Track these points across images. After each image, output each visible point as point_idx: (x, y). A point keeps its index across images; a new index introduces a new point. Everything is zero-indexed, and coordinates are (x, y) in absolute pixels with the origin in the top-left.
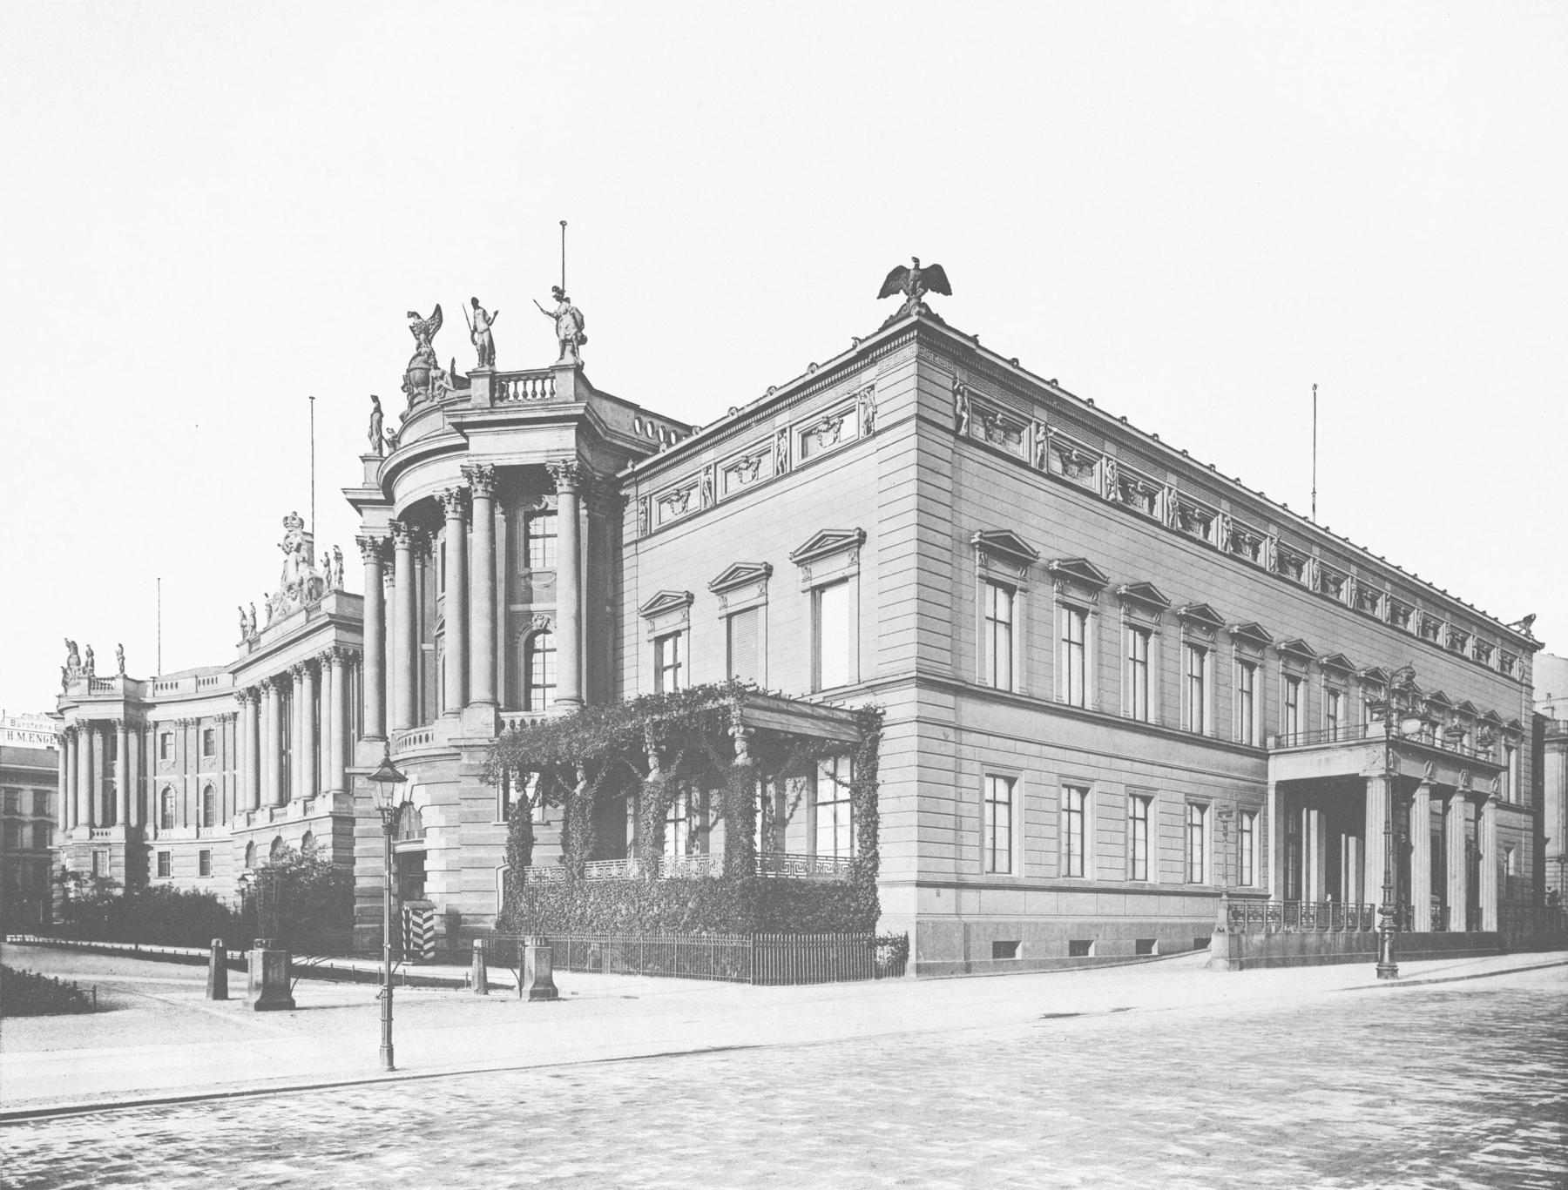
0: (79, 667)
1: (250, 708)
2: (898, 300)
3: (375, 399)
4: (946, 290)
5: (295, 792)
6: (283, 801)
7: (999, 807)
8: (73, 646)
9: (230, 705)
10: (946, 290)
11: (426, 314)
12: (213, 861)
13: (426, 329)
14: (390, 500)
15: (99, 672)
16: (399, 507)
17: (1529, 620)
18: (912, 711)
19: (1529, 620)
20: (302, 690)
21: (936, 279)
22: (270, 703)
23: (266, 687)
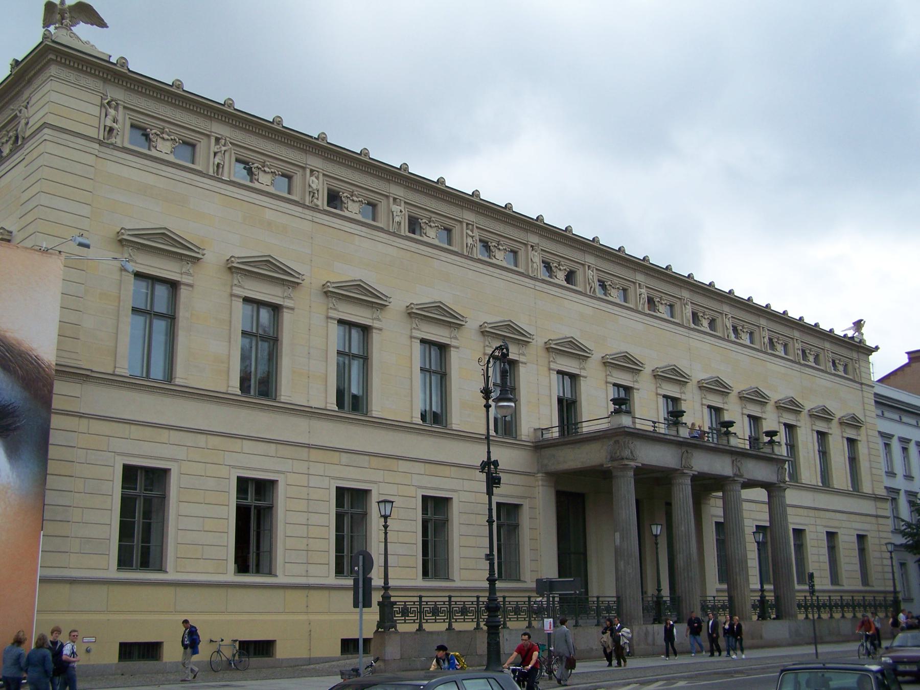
4: (100, 23)
17: (858, 325)
19: (858, 325)
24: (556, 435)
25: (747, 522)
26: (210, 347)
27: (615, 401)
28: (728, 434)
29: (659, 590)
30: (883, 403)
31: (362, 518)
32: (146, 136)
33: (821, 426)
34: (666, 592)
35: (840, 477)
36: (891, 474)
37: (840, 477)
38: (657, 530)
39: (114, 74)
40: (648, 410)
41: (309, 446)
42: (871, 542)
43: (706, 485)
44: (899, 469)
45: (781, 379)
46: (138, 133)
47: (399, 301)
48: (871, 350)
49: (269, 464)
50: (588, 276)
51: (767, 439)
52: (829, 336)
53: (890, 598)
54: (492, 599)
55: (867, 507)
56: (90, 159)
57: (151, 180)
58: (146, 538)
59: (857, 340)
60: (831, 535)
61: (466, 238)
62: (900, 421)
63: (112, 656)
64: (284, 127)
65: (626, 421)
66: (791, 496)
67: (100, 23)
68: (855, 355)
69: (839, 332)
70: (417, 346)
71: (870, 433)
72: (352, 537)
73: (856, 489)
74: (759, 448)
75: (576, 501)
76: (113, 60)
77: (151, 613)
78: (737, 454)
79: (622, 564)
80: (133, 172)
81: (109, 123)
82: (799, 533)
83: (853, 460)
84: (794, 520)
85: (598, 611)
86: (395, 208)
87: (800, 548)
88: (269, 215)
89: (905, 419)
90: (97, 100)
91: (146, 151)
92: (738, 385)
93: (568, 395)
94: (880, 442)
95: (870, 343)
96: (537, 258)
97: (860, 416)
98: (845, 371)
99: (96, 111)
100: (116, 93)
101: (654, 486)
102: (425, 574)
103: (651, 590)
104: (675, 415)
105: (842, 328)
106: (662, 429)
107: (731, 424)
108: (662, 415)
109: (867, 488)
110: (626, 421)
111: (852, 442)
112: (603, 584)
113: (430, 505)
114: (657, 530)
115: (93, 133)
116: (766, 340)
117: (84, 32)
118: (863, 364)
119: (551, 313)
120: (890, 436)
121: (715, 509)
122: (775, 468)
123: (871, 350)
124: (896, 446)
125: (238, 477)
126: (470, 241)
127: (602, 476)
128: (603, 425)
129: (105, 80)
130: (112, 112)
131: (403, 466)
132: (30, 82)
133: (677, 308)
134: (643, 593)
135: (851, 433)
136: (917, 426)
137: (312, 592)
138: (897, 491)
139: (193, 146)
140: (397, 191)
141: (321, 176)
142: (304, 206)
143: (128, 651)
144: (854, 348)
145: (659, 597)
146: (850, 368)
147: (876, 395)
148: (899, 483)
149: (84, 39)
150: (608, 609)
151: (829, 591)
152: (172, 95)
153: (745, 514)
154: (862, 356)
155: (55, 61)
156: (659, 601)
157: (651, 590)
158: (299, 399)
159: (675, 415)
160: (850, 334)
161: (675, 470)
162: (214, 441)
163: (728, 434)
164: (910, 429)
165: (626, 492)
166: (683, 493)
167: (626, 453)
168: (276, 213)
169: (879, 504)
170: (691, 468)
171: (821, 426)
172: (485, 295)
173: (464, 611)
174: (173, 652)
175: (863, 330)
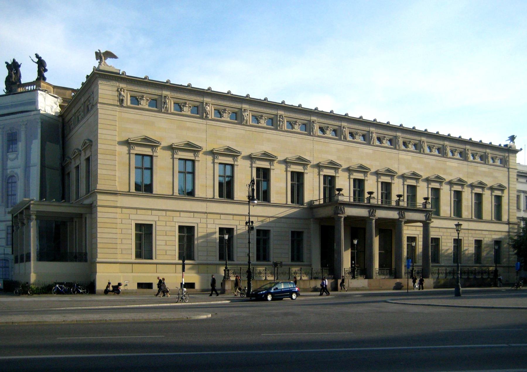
4: (114, 57)
19: (512, 138)
21: (109, 55)
26: (206, 182)
46: (217, 111)
48: (515, 152)
49: (191, 220)
50: (248, 116)
51: (337, 192)
57: (137, 117)
59: (509, 146)
63: (135, 287)
64: (232, 95)
66: (435, 223)
67: (114, 57)
72: (140, 249)
77: (149, 274)
80: (132, 115)
88: (188, 124)
95: (518, 148)
105: (500, 140)
109: (505, 218)
113: (261, 233)
117: (109, 61)
125: (179, 226)
141: (211, 105)
143: (141, 285)
149: (109, 65)
151: (452, 266)
155: (99, 77)
158: (203, 195)
160: (508, 142)
174: (155, 287)
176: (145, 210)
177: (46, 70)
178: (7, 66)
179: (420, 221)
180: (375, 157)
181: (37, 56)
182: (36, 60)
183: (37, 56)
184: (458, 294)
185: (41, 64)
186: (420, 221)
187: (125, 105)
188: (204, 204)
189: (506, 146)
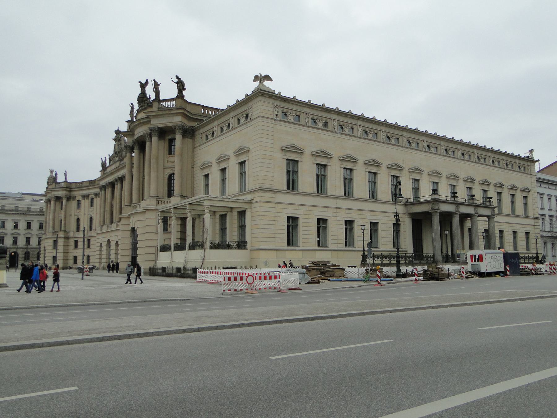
0: (53, 180)
1: (103, 192)
2: (258, 83)
3: (132, 104)
4: (271, 80)
5: (114, 220)
6: (112, 222)
7: (59, 236)
8: (52, 172)
9: (97, 190)
10: (271, 80)
11: (143, 82)
12: (91, 243)
13: (143, 86)
14: (133, 135)
15: (58, 181)
16: (136, 137)
17: (531, 151)
18: (63, 236)
19: (531, 151)
20: (118, 186)
21: (267, 78)
22: (109, 190)
23: (150, 136)
24: (412, 201)
25: (479, 231)
27: (433, 190)
28: (473, 199)
29: (447, 252)
30: (540, 181)
31: (352, 229)
32: (286, 115)
33: (513, 192)
34: (450, 252)
35: (519, 210)
36: (543, 209)
37: (519, 210)
38: (447, 232)
39: (278, 98)
40: (444, 193)
41: (337, 208)
42: (531, 237)
43: (464, 217)
44: (546, 206)
45: (496, 175)
47: (361, 159)
48: (535, 162)
52: (518, 157)
53: (535, 255)
54: (398, 254)
55: (531, 222)
56: (272, 125)
58: (39, 215)
60: (515, 233)
61: (382, 136)
62: (548, 188)
65: (436, 196)
68: (529, 164)
69: (522, 155)
70: (367, 174)
71: (533, 193)
73: (526, 216)
74: (487, 203)
75: (420, 222)
76: (276, 93)
78: (477, 206)
79: (435, 244)
81: (276, 113)
82: (501, 232)
83: (525, 204)
84: (498, 227)
85: (427, 258)
86: (360, 129)
87: (501, 237)
89: (550, 187)
90: (272, 106)
91: (286, 120)
92: (478, 178)
93: (416, 186)
94: (539, 196)
95: (536, 159)
96: (405, 140)
97: (529, 187)
98: (524, 170)
99: (272, 110)
100: (278, 103)
101: (446, 218)
102: (346, 245)
103: (445, 252)
104: (454, 194)
105: (524, 153)
106: (449, 199)
107: (474, 196)
108: (449, 195)
109: (531, 214)
110: (436, 196)
111: (525, 197)
112: (427, 250)
114: (447, 232)
115: (272, 117)
116: (491, 161)
117: (267, 83)
118: (532, 167)
119: (409, 158)
120: (543, 194)
121: (468, 224)
122: (491, 210)
123: (535, 162)
124: (545, 198)
126: (383, 137)
127: (428, 215)
128: (429, 198)
129: (275, 99)
130: (277, 109)
131: (364, 213)
132: (251, 100)
133: (456, 152)
134: (442, 253)
135: (525, 194)
136: (556, 189)
137: (339, 252)
138: (545, 215)
139: (299, 116)
140: (360, 123)
142: (332, 132)
144: (530, 160)
145: (447, 254)
146: (526, 169)
147: (537, 178)
148: (546, 212)
150: (430, 258)
152: (293, 101)
153: (479, 225)
154: (532, 164)
156: (447, 255)
157: (445, 252)
158: (334, 194)
159: (454, 194)
160: (527, 155)
161: (453, 213)
162: (311, 208)
163: (473, 199)
164: (553, 191)
165: (436, 220)
166: (456, 220)
167: (436, 207)
168: (324, 135)
169: (536, 221)
170: (459, 212)
171: (513, 192)
172: (386, 154)
173: (386, 258)
175: (533, 153)
176: (292, 205)
177: (184, 89)
178: (140, 85)
179: (486, 216)
180: (465, 169)
181: (177, 77)
182: (176, 80)
183: (177, 77)
184: (245, 172)
185: (181, 85)
186: (486, 216)
187: (355, 134)
188: (334, 201)
189: (528, 157)
